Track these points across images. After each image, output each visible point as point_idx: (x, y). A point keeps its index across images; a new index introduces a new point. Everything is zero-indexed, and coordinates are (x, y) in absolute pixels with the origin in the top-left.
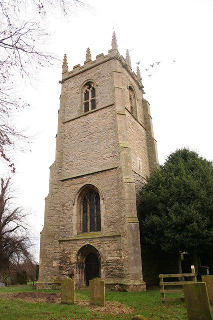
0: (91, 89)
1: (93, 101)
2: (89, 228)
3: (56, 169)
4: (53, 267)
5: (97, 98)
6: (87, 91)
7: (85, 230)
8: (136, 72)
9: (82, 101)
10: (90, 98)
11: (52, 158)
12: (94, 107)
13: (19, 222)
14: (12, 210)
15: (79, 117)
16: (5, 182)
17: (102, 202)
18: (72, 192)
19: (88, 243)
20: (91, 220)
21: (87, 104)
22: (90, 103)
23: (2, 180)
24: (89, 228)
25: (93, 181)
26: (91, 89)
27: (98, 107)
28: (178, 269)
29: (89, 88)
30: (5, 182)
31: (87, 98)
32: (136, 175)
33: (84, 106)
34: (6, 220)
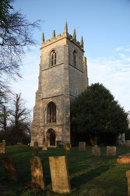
0: (55, 53)
1: (55, 60)
2: (52, 121)
3: (38, 94)
4: (63, 131)
5: (57, 59)
6: (53, 55)
7: (50, 122)
8: (80, 42)
9: (50, 60)
10: (54, 59)
11: (37, 89)
12: (55, 64)
13: (26, 116)
14: (22, 109)
15: (49, 69)
16: (18, 96)
17: (57, 109)
18: (43, 105)
19: (51, 128)
20: (52, 118)
21: (52, 61)
22: (54, 61)
23: (17, 95)
24: (52, 121)
25: (54, 100)
26: (55, 53)
27: (57, 63)
28: (52, 145)
29: (54, 53)
30: (18, 96)
31: (52, 59)
32: (74, 97)
33: (51, 62)
34: (20, 115)
